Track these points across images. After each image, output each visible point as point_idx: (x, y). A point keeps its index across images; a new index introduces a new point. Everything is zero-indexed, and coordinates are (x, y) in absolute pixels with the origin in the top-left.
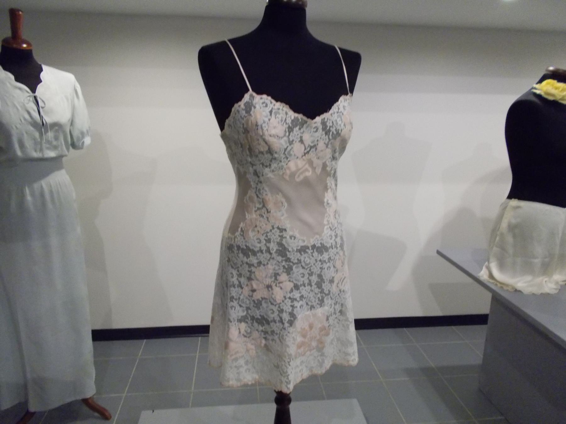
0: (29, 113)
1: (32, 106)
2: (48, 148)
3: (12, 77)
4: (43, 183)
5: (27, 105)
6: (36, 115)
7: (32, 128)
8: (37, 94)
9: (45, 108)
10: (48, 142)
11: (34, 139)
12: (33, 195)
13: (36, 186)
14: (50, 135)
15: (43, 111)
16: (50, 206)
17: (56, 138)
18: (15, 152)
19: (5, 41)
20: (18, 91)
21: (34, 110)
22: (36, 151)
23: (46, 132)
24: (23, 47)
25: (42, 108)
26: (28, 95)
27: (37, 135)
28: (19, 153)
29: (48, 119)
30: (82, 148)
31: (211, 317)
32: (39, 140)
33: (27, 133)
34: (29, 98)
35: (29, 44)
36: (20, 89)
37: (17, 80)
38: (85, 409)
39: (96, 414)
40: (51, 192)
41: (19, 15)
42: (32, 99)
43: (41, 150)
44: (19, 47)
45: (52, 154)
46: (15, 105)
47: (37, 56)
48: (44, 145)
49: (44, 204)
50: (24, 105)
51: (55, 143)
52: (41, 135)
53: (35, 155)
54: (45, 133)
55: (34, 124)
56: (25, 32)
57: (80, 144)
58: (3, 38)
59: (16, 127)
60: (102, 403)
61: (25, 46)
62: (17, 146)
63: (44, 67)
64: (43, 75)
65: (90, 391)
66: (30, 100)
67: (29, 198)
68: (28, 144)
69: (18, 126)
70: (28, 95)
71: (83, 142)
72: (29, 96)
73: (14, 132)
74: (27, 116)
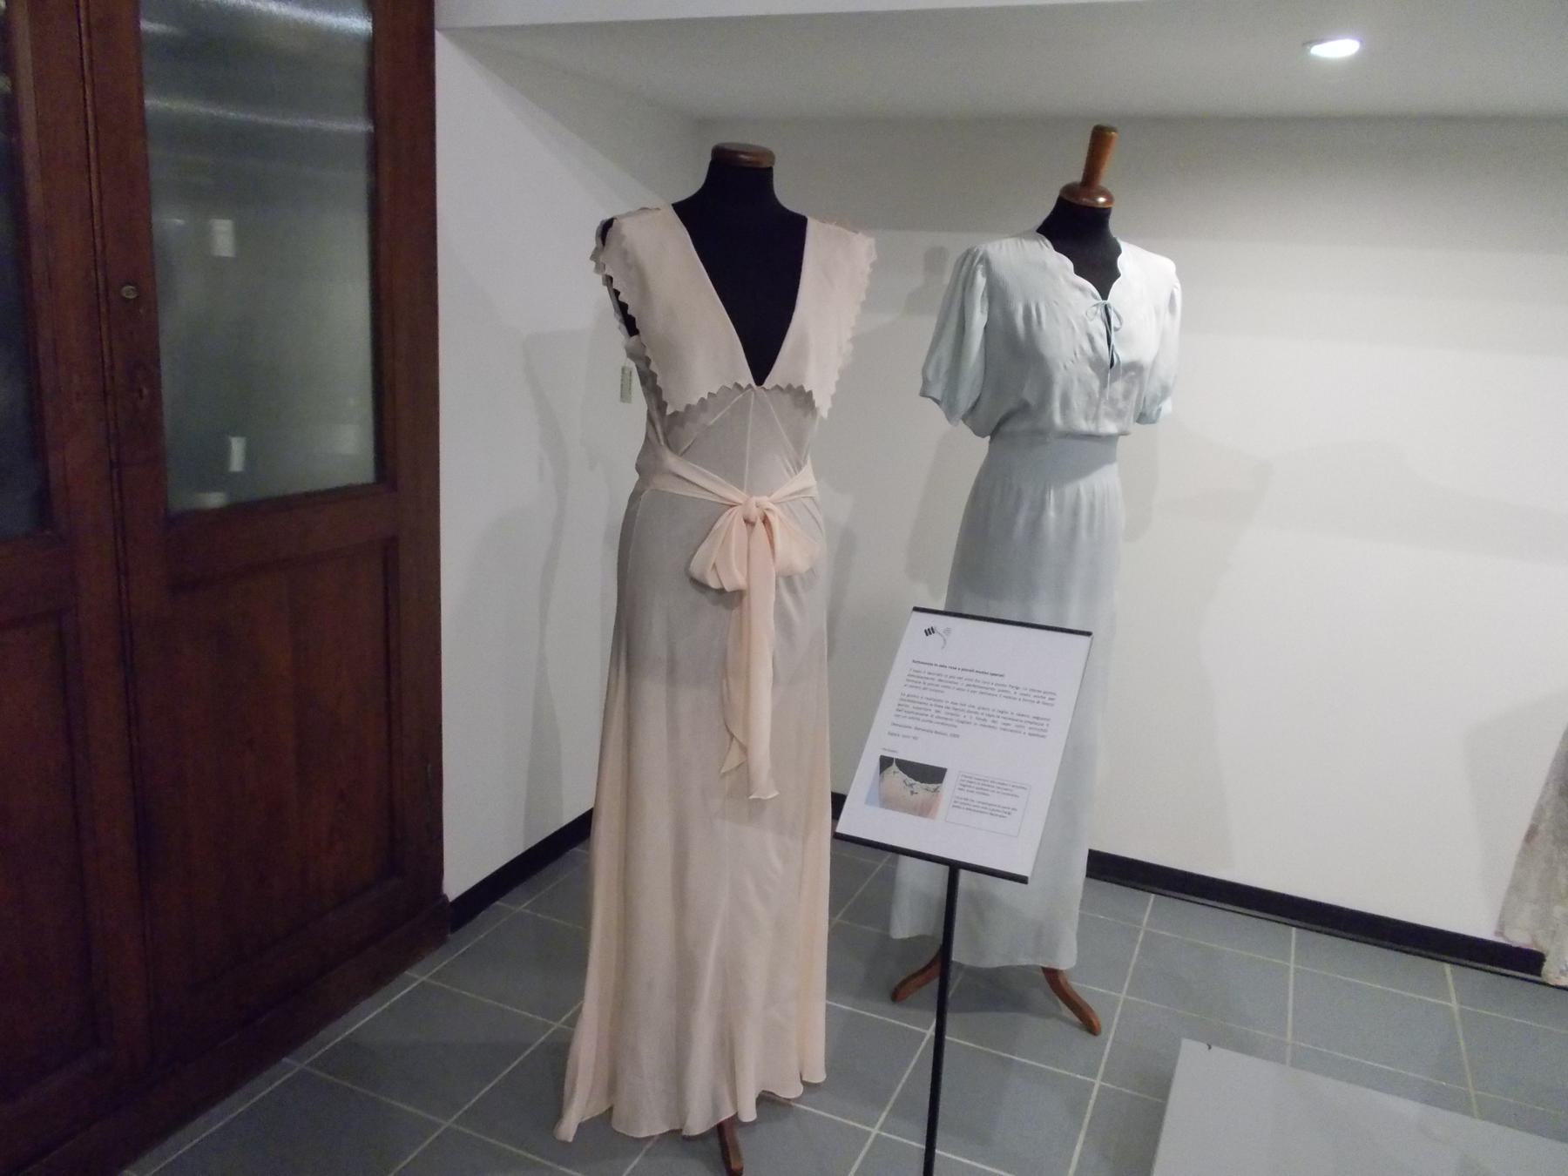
0: (1091, 340)
1: (1098, 326)
2: (1108, 415)
3: (1069, 264)
4: (1083, 485)
5: (1089, 323)
6: (1101, 343)
7: (1089, 371)
8: (1109, 301)
9: (1119, 332)
10: (1113, 402)
11: (1090, 395)
12: (1059, 508)
13: (1069, 490)
14: (1119, 387)
15: (1116, 336)
16: (1083, 534)
17: (1126, 396)
18: (1051, 414)
19: (1068, 190)
20: (1078, 294)
21: (1101, 335)
22: (1086, 418)
23: (1114, 379)
24: (1097, 203)
25: (1116, 330)
26: (1096, 302)
27: (1096, 384)
28: (1058, 419)
29: (1123, 355)
30: (1154, 422)
31: (1533, 807)
32: (1097, 396)
33: (1079, 380)
34: (1095, 308)
35: (1110, 199)
36: (1082, 289)
37: (1078, 271)
38: (1041, 994)
39: (1066, 1012)
40: (1092, 506)
41: (1111, 137)
42: (1101, 311)
43: (1096, 418)
44: (1076, 202)
45: (1110, 427)
46: (1069, 322)
47: (1115, 226)
48: (1104, 408)
49: (1074, 530)
50: (1085, 321)
51: (1121, 405)
52: (1104, 385)
53: (1084, 426)
54: (1112, 381)
55: (1096, 364)
56: (1108, 177)
57: (1154, 412)
58: (715, 144)
59: (1065, 367)
60: (1081, 987)
61: (1102, 200)
62: (1056, 405)
63: (1123, 245)
64: (1123, 262)
65: (1066, 960)
66: (1096, 313)
67: (1051, 513)
68: (1078, 402)
69: (1069, 364)
70: (1096, 302)
71: (1160, 410)
72: (1096, 305)
73: (1059, 377)
74: (1086, 346)
